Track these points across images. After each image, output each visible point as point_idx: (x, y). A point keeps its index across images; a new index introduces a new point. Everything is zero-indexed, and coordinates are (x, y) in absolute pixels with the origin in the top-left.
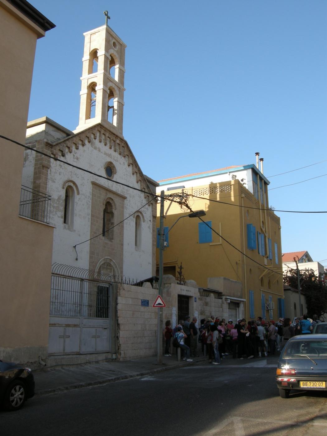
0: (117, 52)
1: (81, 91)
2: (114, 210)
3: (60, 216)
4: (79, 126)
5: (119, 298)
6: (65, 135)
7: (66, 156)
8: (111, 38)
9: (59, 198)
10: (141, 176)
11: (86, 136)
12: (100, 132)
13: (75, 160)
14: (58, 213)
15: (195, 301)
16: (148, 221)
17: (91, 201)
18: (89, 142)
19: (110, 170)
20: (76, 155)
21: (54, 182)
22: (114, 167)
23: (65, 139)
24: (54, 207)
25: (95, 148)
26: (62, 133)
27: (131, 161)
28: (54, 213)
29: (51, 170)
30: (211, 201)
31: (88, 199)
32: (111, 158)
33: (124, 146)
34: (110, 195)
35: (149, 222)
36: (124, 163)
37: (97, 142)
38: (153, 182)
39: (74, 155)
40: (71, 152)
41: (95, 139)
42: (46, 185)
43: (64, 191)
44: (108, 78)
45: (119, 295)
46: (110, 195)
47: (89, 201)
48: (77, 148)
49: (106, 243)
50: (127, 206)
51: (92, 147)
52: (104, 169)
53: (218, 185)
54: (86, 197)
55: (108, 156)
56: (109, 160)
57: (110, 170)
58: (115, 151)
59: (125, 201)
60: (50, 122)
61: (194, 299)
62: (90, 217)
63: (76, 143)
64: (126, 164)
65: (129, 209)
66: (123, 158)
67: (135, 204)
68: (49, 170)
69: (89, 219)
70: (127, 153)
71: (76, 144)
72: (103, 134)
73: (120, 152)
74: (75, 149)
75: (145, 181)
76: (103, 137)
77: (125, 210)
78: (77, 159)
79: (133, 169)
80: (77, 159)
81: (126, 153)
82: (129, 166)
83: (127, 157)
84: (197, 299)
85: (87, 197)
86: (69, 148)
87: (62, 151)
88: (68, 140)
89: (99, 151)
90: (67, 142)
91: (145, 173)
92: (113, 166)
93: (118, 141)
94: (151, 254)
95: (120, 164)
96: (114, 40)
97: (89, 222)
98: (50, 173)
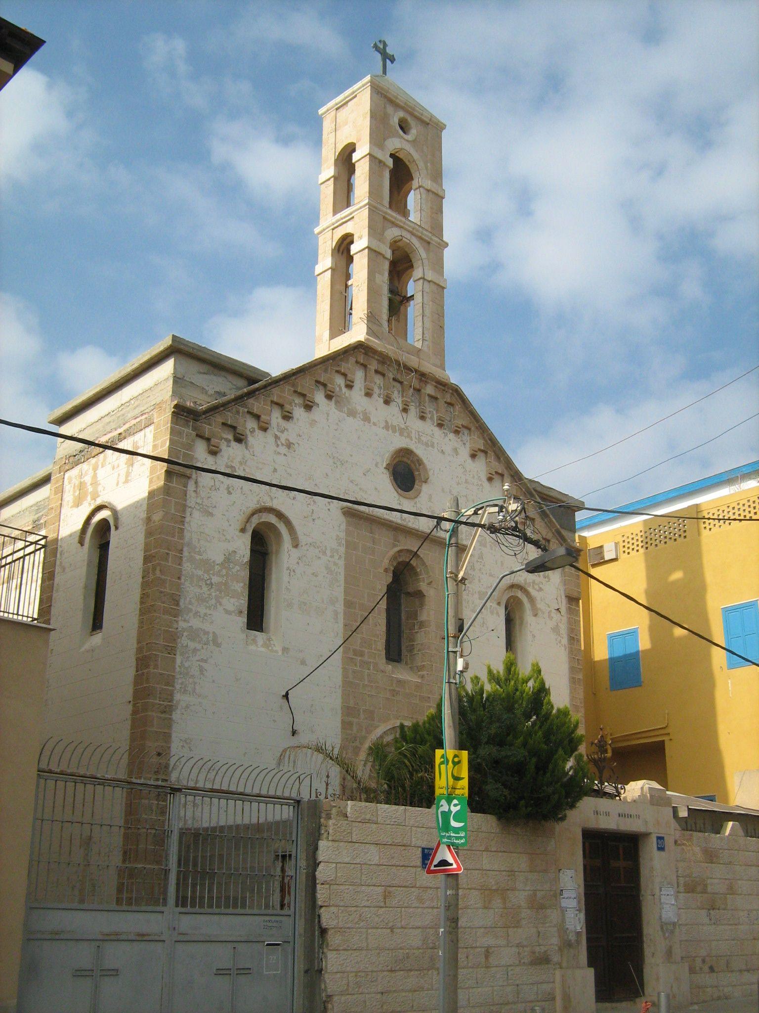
0: (414, 143)
3: (231, 608)
5: (322, 844)
6: (241, 383)
7: (251, 439)
8: (390, 109)
9: (229, 559)
11: (317, 382)
12: (365, 366)
13: (283, 450)
14: (225, 601)
15: (661, 849)
18: (329, 397)
19: (405, 473)
21: (211, 515)
22: (420, 462)
23: (240, 393)
25: (352, 413)
26: (230, 377)
27: (480, 444)
28: (213, 601)
31: (332, 557)
32: (409, 437)
39: (277, 437)
41: (350, 387)
42: (183, 523)
43: (247, 539)
45: (325, 835)
47: (335, 564)
48: (287, 417)
54: (324, 553)
56: (401, 442)
57: (405, 473)
58: (422, 418)
61: (655, 839)
62: (340, 607)
63: (281, 401)
64: (465, 453)
71: (281, 406)
72: (377, 372)
73: (440, 419)
74: (280, 420)
76: (378, 380)
78: (289, 445)
80: (289, 445)
81: (459, 422)
82: (473, 456)
83: (466, 432)
84: (669, 842)
86: (257, 417)
87: (234, 428)
88: (250, 394)
89: (366, 419)
90: (251, 401)
91: (528, 472)
93: (429, 389)
96: (401, 114)
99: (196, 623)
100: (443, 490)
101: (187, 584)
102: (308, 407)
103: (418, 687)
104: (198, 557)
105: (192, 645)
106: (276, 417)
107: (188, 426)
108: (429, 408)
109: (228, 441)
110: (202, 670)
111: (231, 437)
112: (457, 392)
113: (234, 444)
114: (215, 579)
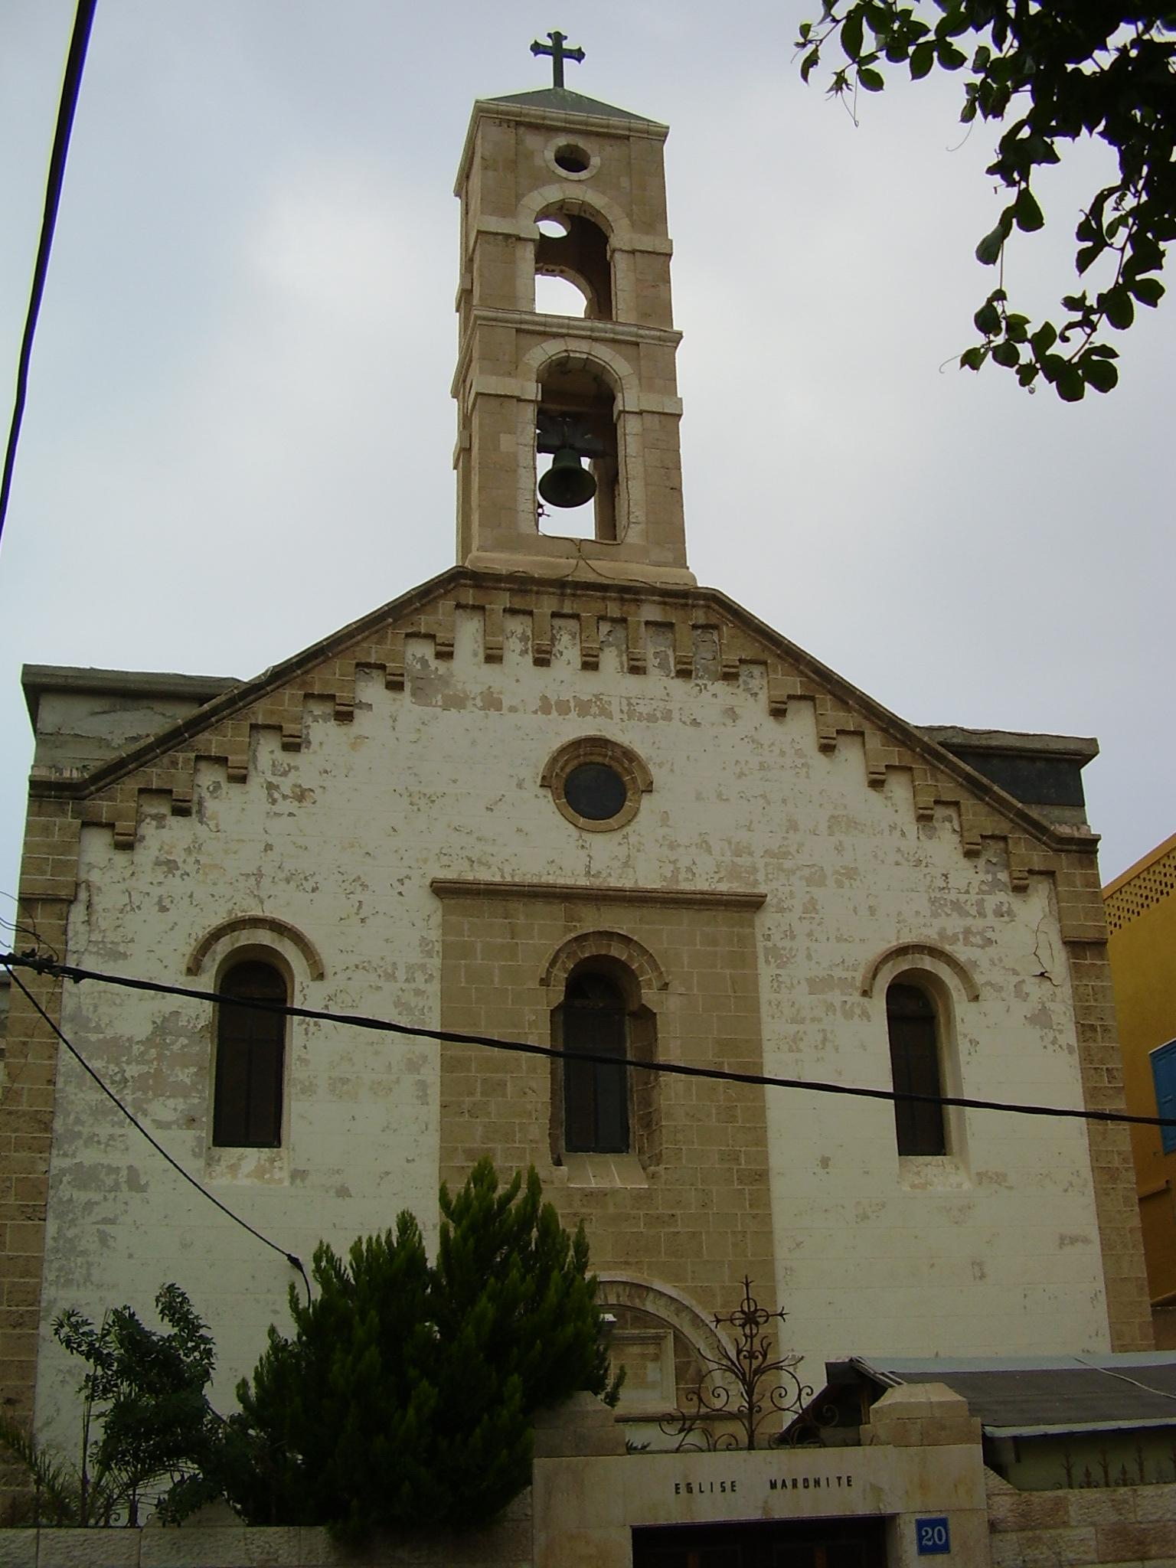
2: (649, 996)
3: (167, 1115)
7: (211, 805)
10: (903, 744)
13: (291, 806)
18: (395, 686)
20: (286, 785)
22: (629, 755)
24: (126, 1081)
30: (1098, 1125)
33: (714, 621)
34: (593, 920)
38: (1054, 746)
39: (271, 787)
44: (518, 330)
46: (593, 920)
47: (418, 993)
50: (787, 943)
53: (747, 930)
57: (595, 783)
59: (766, 920)
67: (872, 910)
68: (78, 913)
70: (735, 647)
75: (941, 758)
77: (766, 972)
79: (818, 717)
90: (205, 736)
91: (917, 710)
92: (618, 753)
94: (1087, 1173)
95: (695, 723)
97: (423, 1099)
98: (88, 922)
99: (88, 1156)
100: (699, 797)
101: (71, 1089)
103: (641, 1198)
104: (93, 1037)
105: (82, 1196)
107: (64, 813)
108: (651, 648)
109: (160, 818)
110: (104, 1239)
111: (165, 809)
112: (715, 600)
113: (173, 821)
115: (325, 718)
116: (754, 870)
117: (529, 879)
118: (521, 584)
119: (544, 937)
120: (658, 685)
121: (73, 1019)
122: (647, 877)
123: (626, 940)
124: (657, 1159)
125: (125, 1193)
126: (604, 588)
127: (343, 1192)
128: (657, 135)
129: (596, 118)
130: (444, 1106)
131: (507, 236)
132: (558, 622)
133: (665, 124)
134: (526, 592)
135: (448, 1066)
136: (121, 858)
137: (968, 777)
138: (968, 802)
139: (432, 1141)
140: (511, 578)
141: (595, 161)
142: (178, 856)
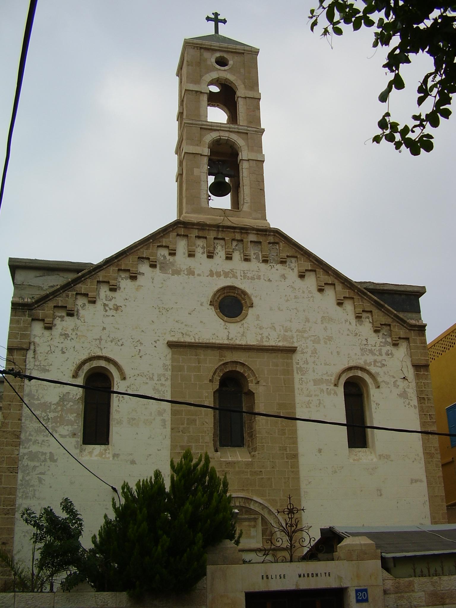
1: (431, 55)
2: (252, 386)
3: (65, 432)
4: (216, 289)
7: (82, 312)
10: (350, 288)
13: (113, 312)
16: (395, 382)
17: (169, 383)
18: (153, 266)
20: (111, 304)
22: (244, 293)
24: (49, 419)
25: (177, 272)
29: (35, 351)
33: (277, 241)
34: (230, 357)
35: (402, 384)
36: (284, 277)
37: (181, 259)
38: (409, 289)
39: (105, 305)
40: (94, 302)
44: (201, 128)
46: (230, 357)
47: (162, 385)
49: (228, 463)
50: (305, 366)
51: (167, 273)
52: (210, 307)
55: (222, 277)
57: (231, 304)
59: (297, 357)
60: (21, 264)
65: (314, 371)
66: (279, 266)
67: (338, 353)
68: (30, 354)
69: (164, 421)
70: (285, 251)
75: (365, 294)
77: (297, 377)
78: (117, 308)
79: (317, 278)
83: (293, 260)
85: (156, 378)
89: (191, 272)
90: (80, 285)
91: (356, 275)
92: (240, 292)
94: (421, 455)
95: (270, 280)
97: (164, 426)
98: (34, 358)
99: (34, 448)
100: (271, 309)
101: (27, 422)
102: (134, 278)
103: (249, 465)
104: (36, 402)
105: (32, 464)
106: (104, 291)
107: (25, 315)
108: (252, 251)
109: (62, 317)
110: (40, 480)
111: (64, 314)
112: (277, 233)
113: (67, 318)
114: (51, 415)
115: (126, 278)
116: (292, 337)
117: (205, 341)
118: (202, 226)
119: (211, 363)
120: (255, 265)
121: (28, 395)
122: (251, 340)
123: (243, 364)
124: (255, 449)
125: (48, 463)
126: (234, 228)
127: (133, 462)
128: (255, 52)
129: (231, 46)
130: (172, 429)
131: (197, 92)
132: (216, 241)
133: (258, 48)
134: (204, 229)
135: (174, 413)
136: (47, 333)
137: (375, 301)
138: (375, 311)
139: (168, 442)
140: (198, 224)
141: (231, 62)
142: (69, 332)
